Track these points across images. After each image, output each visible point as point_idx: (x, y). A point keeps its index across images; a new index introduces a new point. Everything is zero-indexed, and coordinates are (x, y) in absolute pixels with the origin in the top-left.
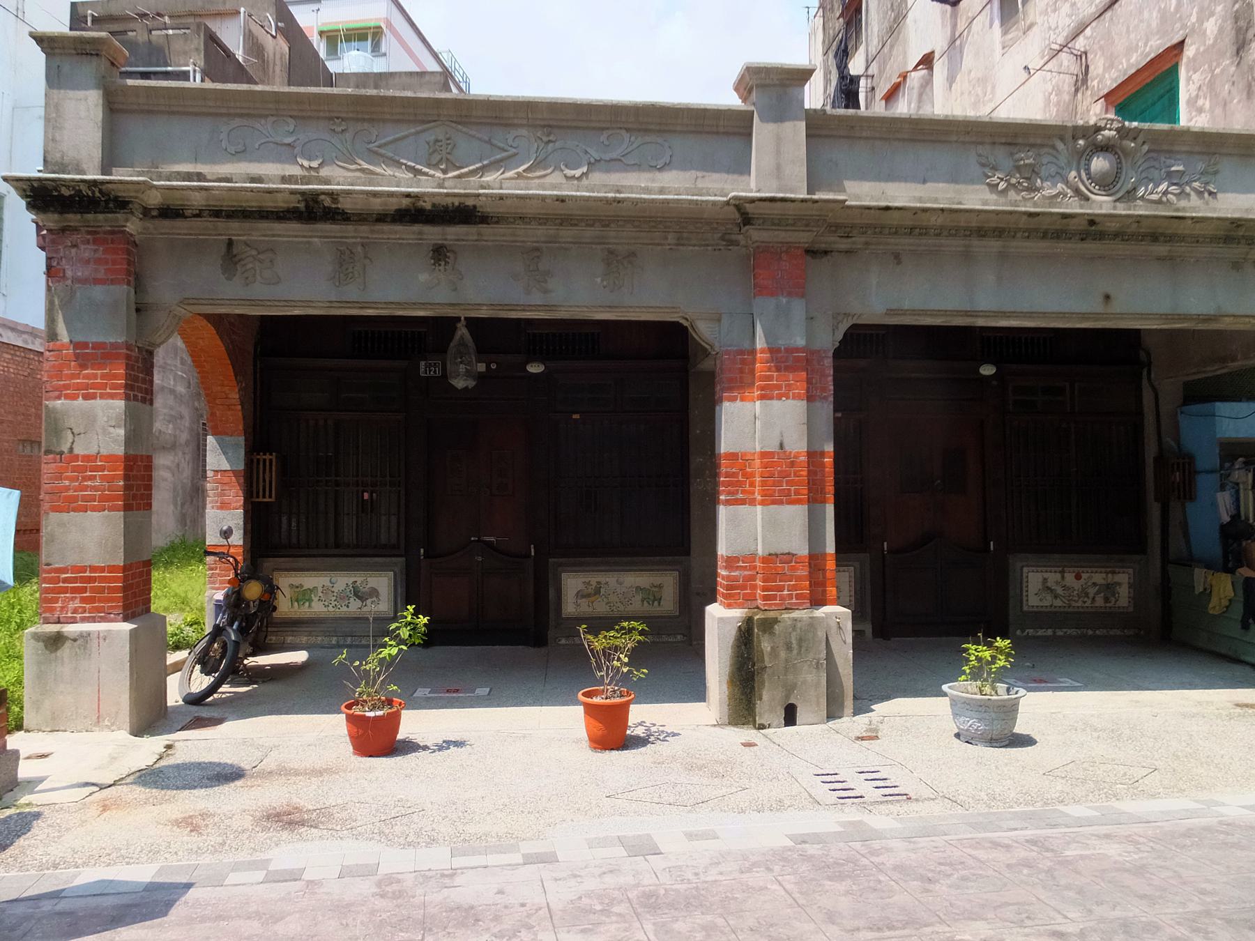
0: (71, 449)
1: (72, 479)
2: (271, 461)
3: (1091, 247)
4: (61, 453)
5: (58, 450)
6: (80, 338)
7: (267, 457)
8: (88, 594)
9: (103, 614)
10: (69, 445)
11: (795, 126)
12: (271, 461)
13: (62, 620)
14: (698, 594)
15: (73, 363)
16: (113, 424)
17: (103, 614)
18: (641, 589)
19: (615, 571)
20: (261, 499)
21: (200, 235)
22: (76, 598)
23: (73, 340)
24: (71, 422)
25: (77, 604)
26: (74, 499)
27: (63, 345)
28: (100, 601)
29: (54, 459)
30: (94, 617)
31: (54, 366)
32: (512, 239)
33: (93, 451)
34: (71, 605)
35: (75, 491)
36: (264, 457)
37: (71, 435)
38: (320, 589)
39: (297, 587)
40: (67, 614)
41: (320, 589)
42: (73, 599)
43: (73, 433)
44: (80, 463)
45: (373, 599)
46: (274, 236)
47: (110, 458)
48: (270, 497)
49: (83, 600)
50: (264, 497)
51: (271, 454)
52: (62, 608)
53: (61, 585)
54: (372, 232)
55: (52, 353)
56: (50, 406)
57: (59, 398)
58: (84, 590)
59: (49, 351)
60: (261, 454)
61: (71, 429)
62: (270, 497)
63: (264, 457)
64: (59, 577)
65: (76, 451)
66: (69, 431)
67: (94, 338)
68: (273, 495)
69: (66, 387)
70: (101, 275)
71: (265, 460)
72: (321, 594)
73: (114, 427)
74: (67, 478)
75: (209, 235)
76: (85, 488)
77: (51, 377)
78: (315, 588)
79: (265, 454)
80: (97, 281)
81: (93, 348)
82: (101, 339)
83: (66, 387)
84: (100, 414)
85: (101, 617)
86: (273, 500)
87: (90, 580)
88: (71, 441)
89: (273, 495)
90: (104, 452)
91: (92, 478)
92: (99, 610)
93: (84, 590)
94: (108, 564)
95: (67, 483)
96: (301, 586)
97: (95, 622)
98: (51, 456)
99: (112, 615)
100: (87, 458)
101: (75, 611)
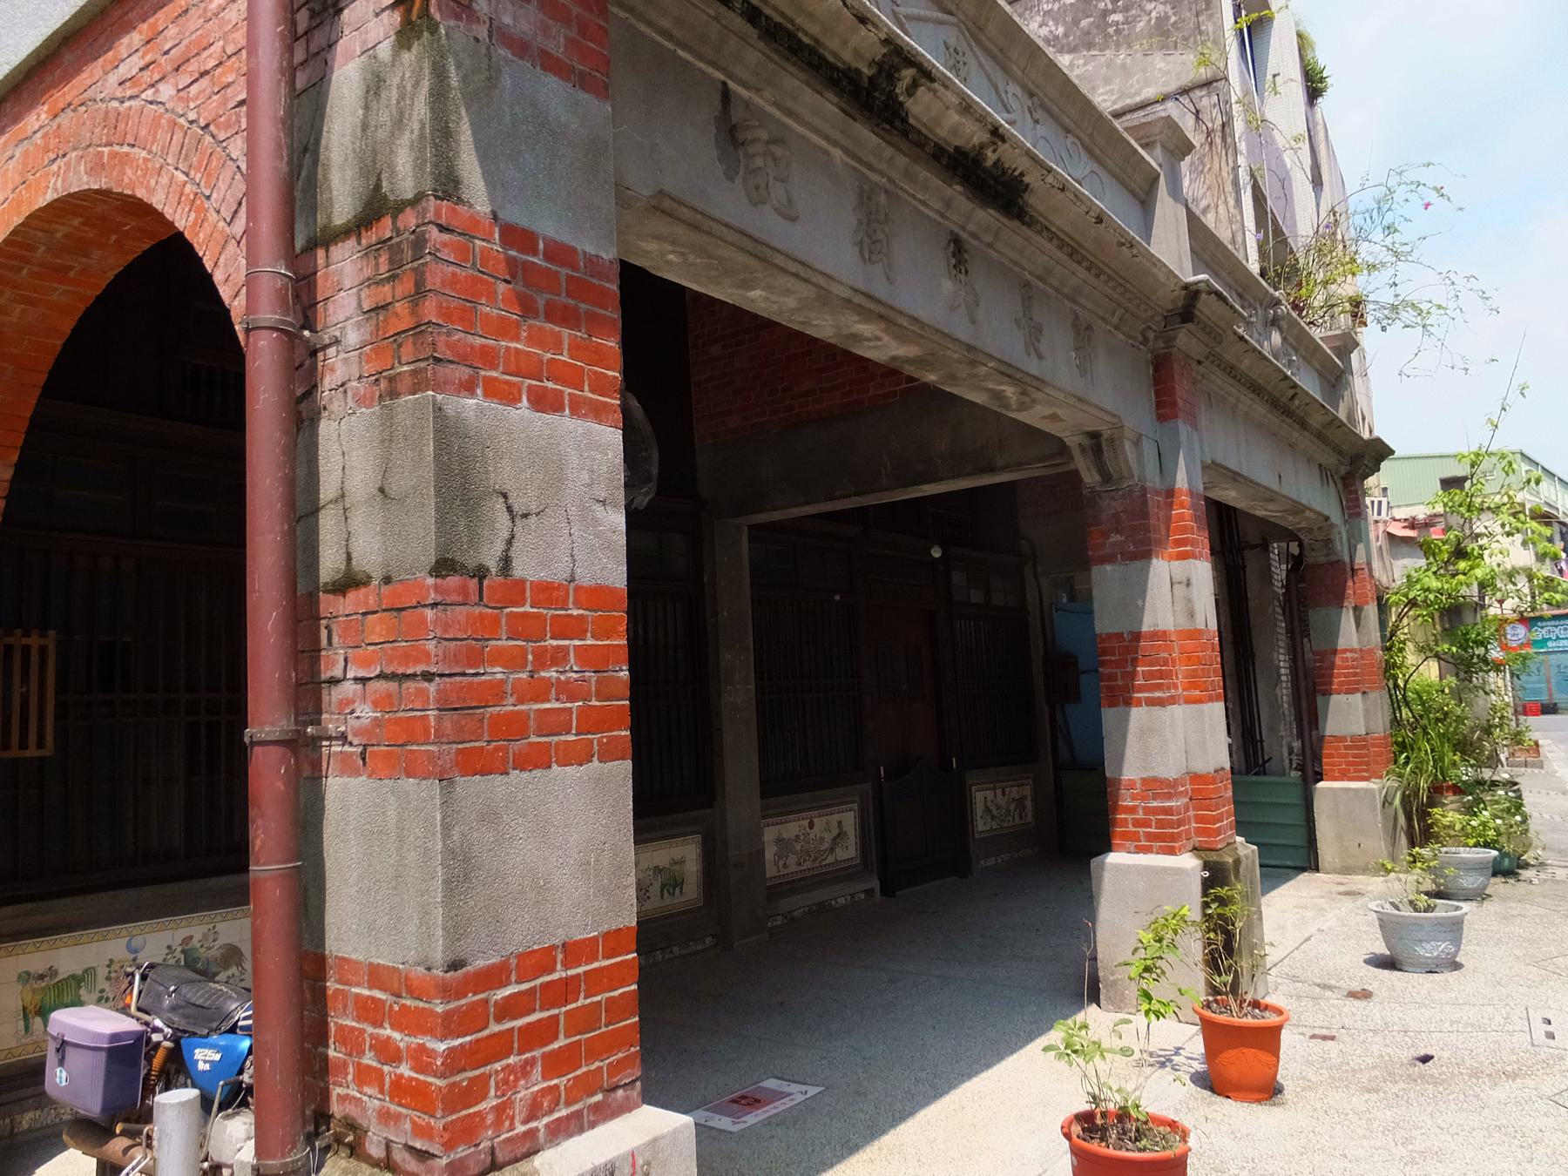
0: (506, 562)
1: (513, 661)
2: (43, 650)
3: (1274, 420)
4: (481, 573)
5: (471, 563)
6: (515, 215)
7: (34, 641)
8: (561, 1042)
9: (599, 1097)
10: (499, 547)
11: (973, 209)
12: (43, 650)
13: (501, 1156)
14: (736, 866)
15: (502, 288)
16: (602, 495)
17: (599, 1097)
18: (660, 871)
19: (678, 836)
20: (32, 752)
21: (684, 47)
22: (531, 1062)
23: (501, 215)
24: (504, 474)
25: (537, 1083)
26: (513, 727)
27: (474, 221)
28: (593, 1055)
29: (463, 590)
30: (577, 1115)
31: (453, 281)
32: (1014, 256)
33: (557, 572)
34: (523, 1094)
35: (521, 701)
36: (25, 641)
37: (504, 518)
38: (102, 973)
39: (41, 977)
40: (512, 1128)
41: (102, 973)
42: (525, 1070)
43: (509, 509)
44: (527, 609)
45: (229, 973)
46: (790, 113)
47: (595, 596)
48: (41, 744)
49: (556, 1064)
50: (23, 745)
51: (43, 635)
52: (500, 1110)
53: (495, 1028)
54: (907, 175)
55: (446, 237)
56: (449, 410)
57: (468, 387)
58: (546, 1031)
59: (443, 229)
60: (18, 632)
61: (505, 496)
62: (41, 744)
63: (25, 641)
64: (486, 1001)
65: (520, 570)
66: (500, 505)
67: (548, 228)
68: (49, 739)
69: (488, 357)
70: (557, 47)
71: (26, 650)
72: (106, 985)
73: (603, 502)
74: (499, 657)
75: (700, 57)
76: (540, 691)
77: (447, 315)
78: (90, 972)
79: (27, 634)
80: (550, 64)
81: (548, 257)
82: (565, 237)
83: (488, 357)
84: (574, 460)
85: (596, 1108)
86: (48, 751)
87: (567, 989)
88: (506, 534)
89: (49, 739)
90: (585, 578)
91: (559, 657)
92: (586, 1086)
93: (546, 1031)
94: (606, 928)
95: (497, 672)
96: (53, 972)
97: (581, 1130)
98: (453, 581)
99: (620, 1092)
100: (548, 593)
101: (534, 1112)
